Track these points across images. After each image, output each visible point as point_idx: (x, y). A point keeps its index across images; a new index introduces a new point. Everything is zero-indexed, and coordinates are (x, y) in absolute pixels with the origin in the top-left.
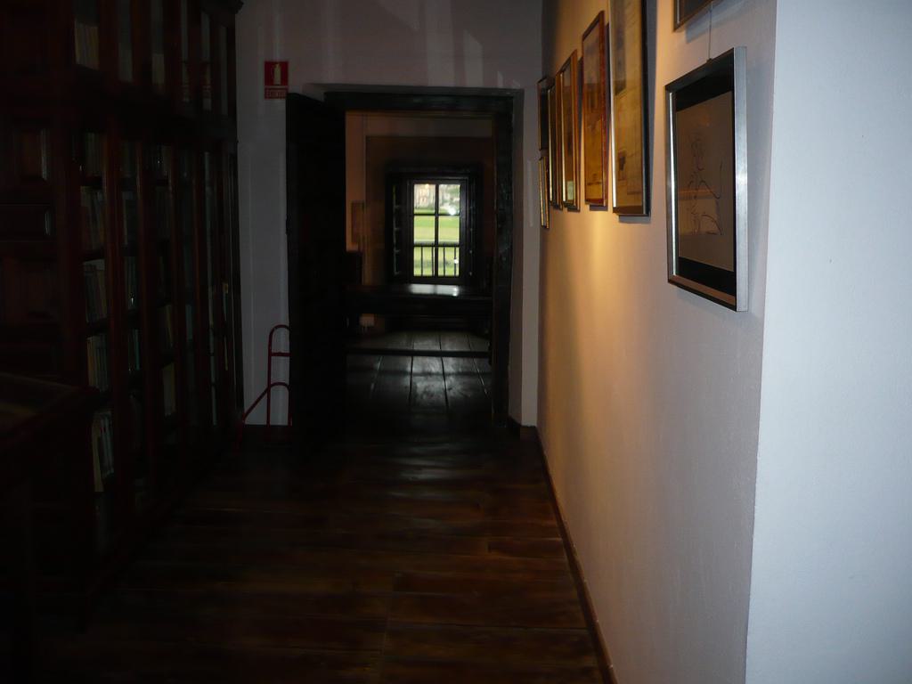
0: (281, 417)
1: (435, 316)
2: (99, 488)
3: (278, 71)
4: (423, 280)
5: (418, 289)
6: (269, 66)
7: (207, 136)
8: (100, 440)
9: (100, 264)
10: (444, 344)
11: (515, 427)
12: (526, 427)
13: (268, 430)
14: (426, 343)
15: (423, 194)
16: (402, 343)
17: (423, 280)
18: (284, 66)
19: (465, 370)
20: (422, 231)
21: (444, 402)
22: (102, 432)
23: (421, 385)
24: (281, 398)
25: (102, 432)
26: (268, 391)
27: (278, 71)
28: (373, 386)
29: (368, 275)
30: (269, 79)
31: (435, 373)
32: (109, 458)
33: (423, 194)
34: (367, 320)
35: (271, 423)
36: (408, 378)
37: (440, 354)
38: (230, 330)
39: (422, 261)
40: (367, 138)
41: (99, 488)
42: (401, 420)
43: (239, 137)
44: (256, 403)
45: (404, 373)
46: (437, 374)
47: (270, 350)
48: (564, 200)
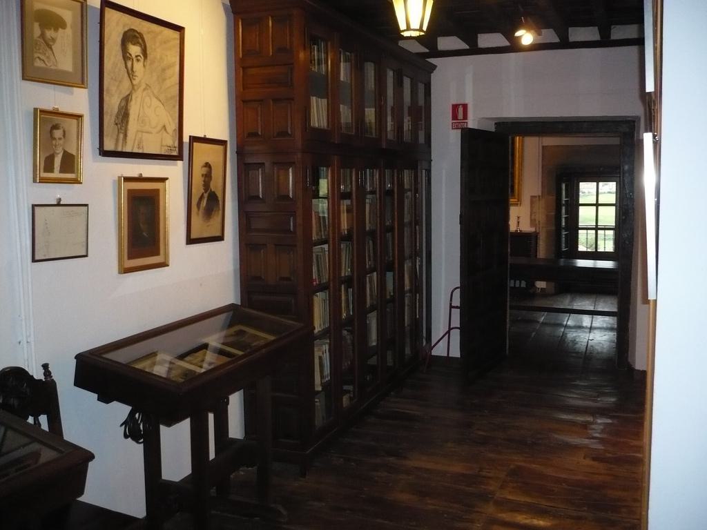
0: (456, 352)
1: (595, 284)
2: (318, 388)
3: (461, 110)
4: (586, 255)
5: (582, 263)
6: (455, 107)
7: (411, 155)
8: (320, 358)
9: (523, 284)
10: (598, 305)
11: (631, 369)
12: (639, 371)
13: (448, 359)
14: (584, 303)
15: (587, 190)
16: (565, 303)
17: (586, 255)
18: (465, 107)
19: (609, 326)
20: (586, 216)
21: (585, 349)
22: (322, 352)
23: (571, 335)
24: (456, 336)
25: (322, 352)
26: (448, 332)
27: (461, 110)
28: (534, 334)
29: (542, 252)
30: (455, 117)
31: (592, 331)
32: (327, 371)
33: (587, 190)
34: (541, 285)
35: (450, 355)
36: (562, 330)
37: (593, 313)
38: (422, 286)
39: (584, 241)
40: (543, 147)
41: (318, 388)
42: (565, 363)
43: (433, 156)
44: (439, 341)
45: (560, 325)
46: (586, 327)
47: (451, 304)
48: (395, 171)
